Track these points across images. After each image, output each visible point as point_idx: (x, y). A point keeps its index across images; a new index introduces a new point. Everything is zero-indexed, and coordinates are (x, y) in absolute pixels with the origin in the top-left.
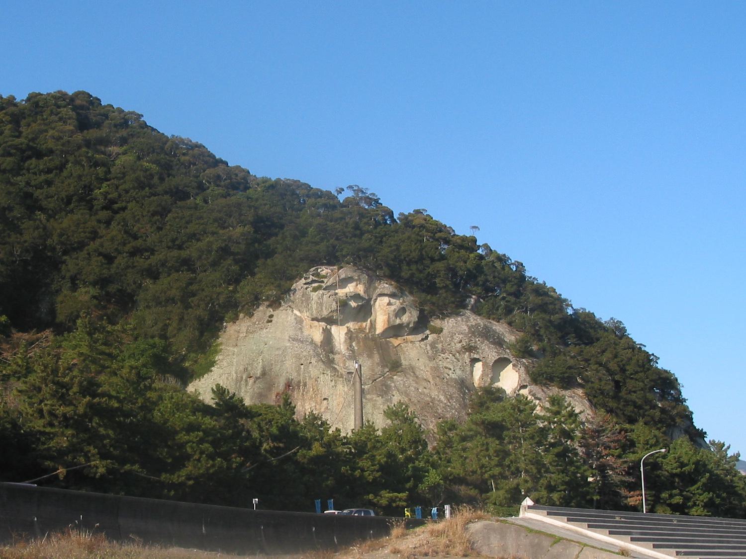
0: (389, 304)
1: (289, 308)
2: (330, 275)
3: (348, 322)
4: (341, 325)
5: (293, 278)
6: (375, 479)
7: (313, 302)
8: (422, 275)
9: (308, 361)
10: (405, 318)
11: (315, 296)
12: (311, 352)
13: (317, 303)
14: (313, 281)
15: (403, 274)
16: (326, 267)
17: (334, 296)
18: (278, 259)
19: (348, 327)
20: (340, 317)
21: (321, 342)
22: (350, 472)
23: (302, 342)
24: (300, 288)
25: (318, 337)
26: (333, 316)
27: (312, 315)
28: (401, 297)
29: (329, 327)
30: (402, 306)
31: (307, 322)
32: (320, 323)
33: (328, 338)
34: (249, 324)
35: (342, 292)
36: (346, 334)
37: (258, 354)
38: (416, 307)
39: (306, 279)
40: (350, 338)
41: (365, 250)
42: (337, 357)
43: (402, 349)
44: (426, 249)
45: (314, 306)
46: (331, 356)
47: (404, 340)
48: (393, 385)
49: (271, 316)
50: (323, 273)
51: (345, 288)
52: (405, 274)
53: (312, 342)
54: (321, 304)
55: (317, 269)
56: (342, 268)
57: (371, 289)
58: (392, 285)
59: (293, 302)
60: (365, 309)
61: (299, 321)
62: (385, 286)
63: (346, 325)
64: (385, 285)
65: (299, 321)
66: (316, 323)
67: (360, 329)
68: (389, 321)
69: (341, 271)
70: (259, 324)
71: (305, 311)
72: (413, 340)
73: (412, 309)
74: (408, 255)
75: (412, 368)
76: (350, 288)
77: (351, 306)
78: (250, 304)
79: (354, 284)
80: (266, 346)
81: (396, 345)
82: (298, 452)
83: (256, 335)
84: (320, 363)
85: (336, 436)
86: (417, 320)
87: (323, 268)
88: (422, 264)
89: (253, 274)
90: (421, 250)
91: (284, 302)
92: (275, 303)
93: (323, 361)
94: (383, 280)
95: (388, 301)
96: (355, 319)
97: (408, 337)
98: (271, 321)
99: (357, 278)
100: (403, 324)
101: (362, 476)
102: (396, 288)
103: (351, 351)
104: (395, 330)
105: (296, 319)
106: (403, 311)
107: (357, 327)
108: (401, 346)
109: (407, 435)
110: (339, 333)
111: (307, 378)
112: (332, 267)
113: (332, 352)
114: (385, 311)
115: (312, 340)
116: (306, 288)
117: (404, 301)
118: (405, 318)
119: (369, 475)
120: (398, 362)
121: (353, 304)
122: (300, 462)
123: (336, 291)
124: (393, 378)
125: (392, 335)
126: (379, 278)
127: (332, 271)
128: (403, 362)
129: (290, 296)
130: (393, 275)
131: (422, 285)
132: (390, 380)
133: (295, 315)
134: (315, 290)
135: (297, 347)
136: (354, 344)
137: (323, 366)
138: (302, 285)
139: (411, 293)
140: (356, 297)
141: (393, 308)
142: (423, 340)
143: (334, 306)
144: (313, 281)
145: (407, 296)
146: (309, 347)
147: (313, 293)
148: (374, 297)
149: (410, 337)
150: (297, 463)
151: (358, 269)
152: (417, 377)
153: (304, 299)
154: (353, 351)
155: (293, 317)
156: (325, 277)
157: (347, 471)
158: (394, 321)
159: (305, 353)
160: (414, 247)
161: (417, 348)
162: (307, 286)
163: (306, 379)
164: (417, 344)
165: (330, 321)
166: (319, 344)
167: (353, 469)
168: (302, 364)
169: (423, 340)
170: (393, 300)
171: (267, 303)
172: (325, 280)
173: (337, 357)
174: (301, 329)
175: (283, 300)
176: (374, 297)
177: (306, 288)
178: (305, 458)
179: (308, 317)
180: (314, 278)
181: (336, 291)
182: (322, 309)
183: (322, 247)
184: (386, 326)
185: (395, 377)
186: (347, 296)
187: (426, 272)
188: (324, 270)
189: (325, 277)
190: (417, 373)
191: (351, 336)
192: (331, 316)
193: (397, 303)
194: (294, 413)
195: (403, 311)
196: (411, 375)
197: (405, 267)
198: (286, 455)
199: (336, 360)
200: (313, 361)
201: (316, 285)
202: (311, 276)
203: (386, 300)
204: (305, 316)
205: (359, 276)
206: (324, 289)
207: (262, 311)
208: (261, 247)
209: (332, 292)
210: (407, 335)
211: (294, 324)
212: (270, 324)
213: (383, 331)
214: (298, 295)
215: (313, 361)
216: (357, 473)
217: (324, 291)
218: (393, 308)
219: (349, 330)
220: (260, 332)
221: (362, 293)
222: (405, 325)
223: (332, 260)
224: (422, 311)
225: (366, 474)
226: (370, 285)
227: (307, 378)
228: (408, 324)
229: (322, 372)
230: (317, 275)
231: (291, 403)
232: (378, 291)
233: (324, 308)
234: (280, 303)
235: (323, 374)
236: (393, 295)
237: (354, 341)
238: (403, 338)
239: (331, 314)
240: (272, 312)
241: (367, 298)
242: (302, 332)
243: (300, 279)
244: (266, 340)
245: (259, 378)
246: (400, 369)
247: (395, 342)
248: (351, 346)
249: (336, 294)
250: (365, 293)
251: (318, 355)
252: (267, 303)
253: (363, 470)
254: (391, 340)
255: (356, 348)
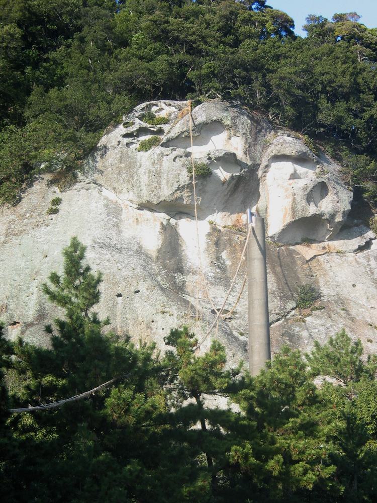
0: (294, 176)
1: (92, 185)
2: (176, 117)
3: (213, 212)
4: (199, 219)
5: (98, 127)
6: (320, 483)
7: (142, 171)
8: (358, 120)
9: (133, 289)
10: (326, 205)
11: (145, 158)
12: (139, 270)
13: (150, 172)
14: (142, 131)
15: (320, 116)
16: (167, 101)
17: (184, 159)
18: (72, 93)
19: (211, 223)
20: (197, 201)
21: (159, 251)
22: (253, 460)
23: (119, 250)
24: (115, 143)
25: (152, 241)
26: (181, 198)
27: (140, 197)
28: (318, 163)
29: (173, 221)
30: (320, 180)
31: (130, 213)
32: (156, 214)
33: (172, 244)
34: (11, 217)
35: (199, 152)
36: (209, 235)
37: (30, 276)
38: (348, 184)
39: (126, 125)
40: (217, 244)
41: (244, 66)
42: (190, 279)
43: (320, 265)
44: (365, 74)
45: (145, 179)
46: (179, 278)
47: (324, 248)
48: (305, 334)
49: (57, 202)
50: (162, 114)
51: (206, 143)
52: (327, 114)
53: (140, 251)
54: (157, 174)
55: (149, 107)
56: (199, 102)
57: (258, 147)
58: (299, 138)
59: (102, 172)
60: (244, 186)
61: (114, 211)
62: (287, 142)
63: (211, 218)
64: (286, 138)
65: (114, 211)
66: (146, 213)
67: (234, 226)
68: (294, 210)
69: (197, 108)
70: (31, 216)
71: (125, 190)
72: (340, 249)
73: (338, 187)
74: (331, 82)
75: (343, 303)
76: (219, 143)
77: (218, 178)
78: (13, 180)
79: (224, 135)
80: (48, 259)
81: (308, 259)
82: (108, 394)
83: (26, 240)
84: (157, 292)
85: (214, 363)
86: (350, 208)
87: (162, 103)
88: (359, 100)
89: (21, 122)
90: (355, 74)
91: (84, 173)
92: (66, 175)
93: (162, 289)
94: (281, 129)
95: (292, 171)
96: (227, 207)
97: (331, 243)
98: (56, 211)
99: (229, 122)
100: (321, 215)
101: (285, 476)
102: (307, 144)
103: (220, 268)
104: (307, 228)
105: (107, 206)
106: (321, 189)
107: (230, 223)
108: (319, 261)
109: (368, 402)
110: (194, 234)
111: (131, 323)
112: (179, 103)
113: (180, 270)
114: (287, 190)
115: (141, 247)
116: (128, 145)
117: (323, 172)
118: (326, 205)
119: (305, 472)
120: (313, 290)
121: (222, 174)
122: (113, 424)
123: (188, 150)
124: (304, 321)
125: (299, 240)
126: (274, 127)
127: (180, 110)
128: (324, 290)
129: (94, 160)
130: (301, 121)
131: (359, 141)
132: (300, 326)
133: (106, 198)
134: (145, 147)
135: (108, 260)
136: (224, 255)
137: (162, 298)
138: (121, 139)
139: (337, 158)
140: (229, 159)
141: (301, 183)
142: (361, 249)
143: (184, 178)
144: (142, 131)
145: (329, 163)
146: (134, 261)
147: (142, 153)
148: (264, 163)
149: (337, 244)
150: (104, 425)
151: (233, 106)
152: (353, 319)
153: (123, 165)
154: (222, 268)
155: (102, 202)
156: (166, 121)
157: (246, 457)
158: (304, 209)
159: (125, 273)
160: (340, 67)
161: (350, 264)
162: (130, 140)
163: (127, 325)
164: (351, 257)
165: (175, 209)
166: (154, 254)
167: (263, 455)
168: (119, 295)
169: (361, 249)
170: (301, 170)
171: (48, 177)
172: (166, 128)
173: (190, 279)
174: (117, 225)
175: (81, 168)
176: (264, 163)
177: (128, 145)
178: (127, 411)
179: (131, 201)
180: (144, 124)
181: (188, 150)
182: (159, 184)
183: (160, 64)
184: (289, 219)
185: (308, 319)
186: (209, 159)
187: (366, 116)
188: (164, 108)
189: (166, 121)
190: (353, 312)
191: (218, 239)
192: (176, 199)
193: (309, 176)
194: (95, 298)
195: (321, 189)
196: (341, 316)
197: (323, 103)
198: (72, 399)
199: (189, 287)
200: (143, 287)
201: (147, 137)
202: (137, 121)
203: (288, 167)
204: (126, 199)
205: (233, 119)
206: (162, 145)
207: (39, 193)
208: (38, 73)
209: (180, 151)
210: (330, 239)
211: (104, 216)
212: (53, 216)
213: (283, 230)
214: (112, 156)
215: (143, 287)
216: (274, 465)
217: (163, 149)
218: (301, 183)
219: (215, 229)
220: (33, 233)
221: (240, 155)
222: (326, 217)
223: (178, 88)
224: (358, 193)
225: (299, 468)
226: (255, 139)
227: (131, 323)
228: (333, 216)
229: (161, 309)
230: (151, 118)
231: (88, 269)
232: (272, 150)
233: (164, 182)
234: (75, 177)
235: (163, 313)
236: (301, 159)
237: (225, 249)
238: (322, 244)
239: (178, 194)
240: (59, 195)
241: (249, 163)
242: (120, 232)
243: (115, 127)
244: (46, 247)
245: (31, 325)
246: (317, 304)
247: (306, 252)
248: (218, 258)
249: (188, 155)
250: (245, 153)
251: (152, 276)
252: (48, 177)
253: (289, 461)
254: (298, 248)
255: (228, 263)
